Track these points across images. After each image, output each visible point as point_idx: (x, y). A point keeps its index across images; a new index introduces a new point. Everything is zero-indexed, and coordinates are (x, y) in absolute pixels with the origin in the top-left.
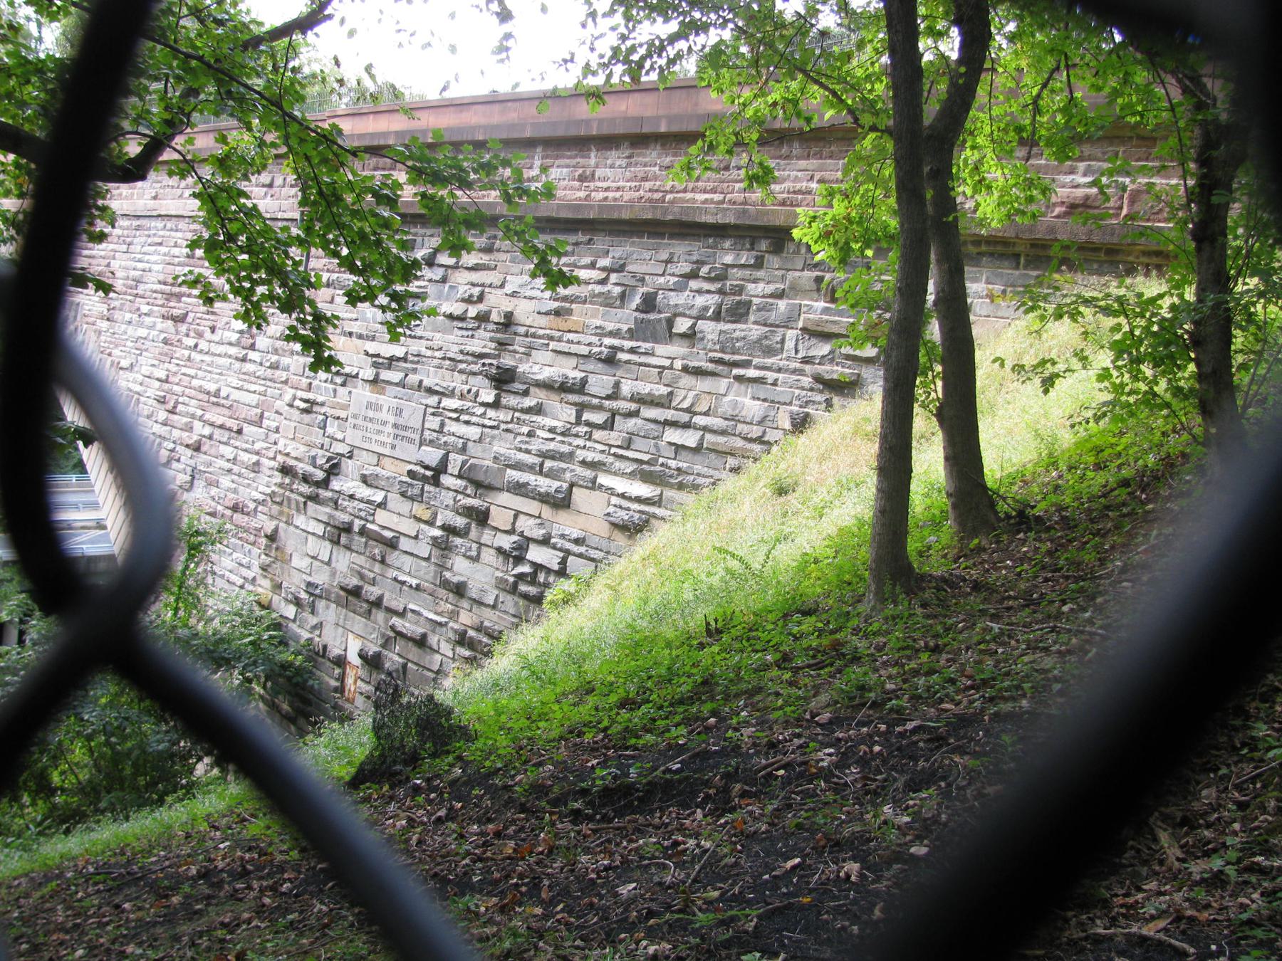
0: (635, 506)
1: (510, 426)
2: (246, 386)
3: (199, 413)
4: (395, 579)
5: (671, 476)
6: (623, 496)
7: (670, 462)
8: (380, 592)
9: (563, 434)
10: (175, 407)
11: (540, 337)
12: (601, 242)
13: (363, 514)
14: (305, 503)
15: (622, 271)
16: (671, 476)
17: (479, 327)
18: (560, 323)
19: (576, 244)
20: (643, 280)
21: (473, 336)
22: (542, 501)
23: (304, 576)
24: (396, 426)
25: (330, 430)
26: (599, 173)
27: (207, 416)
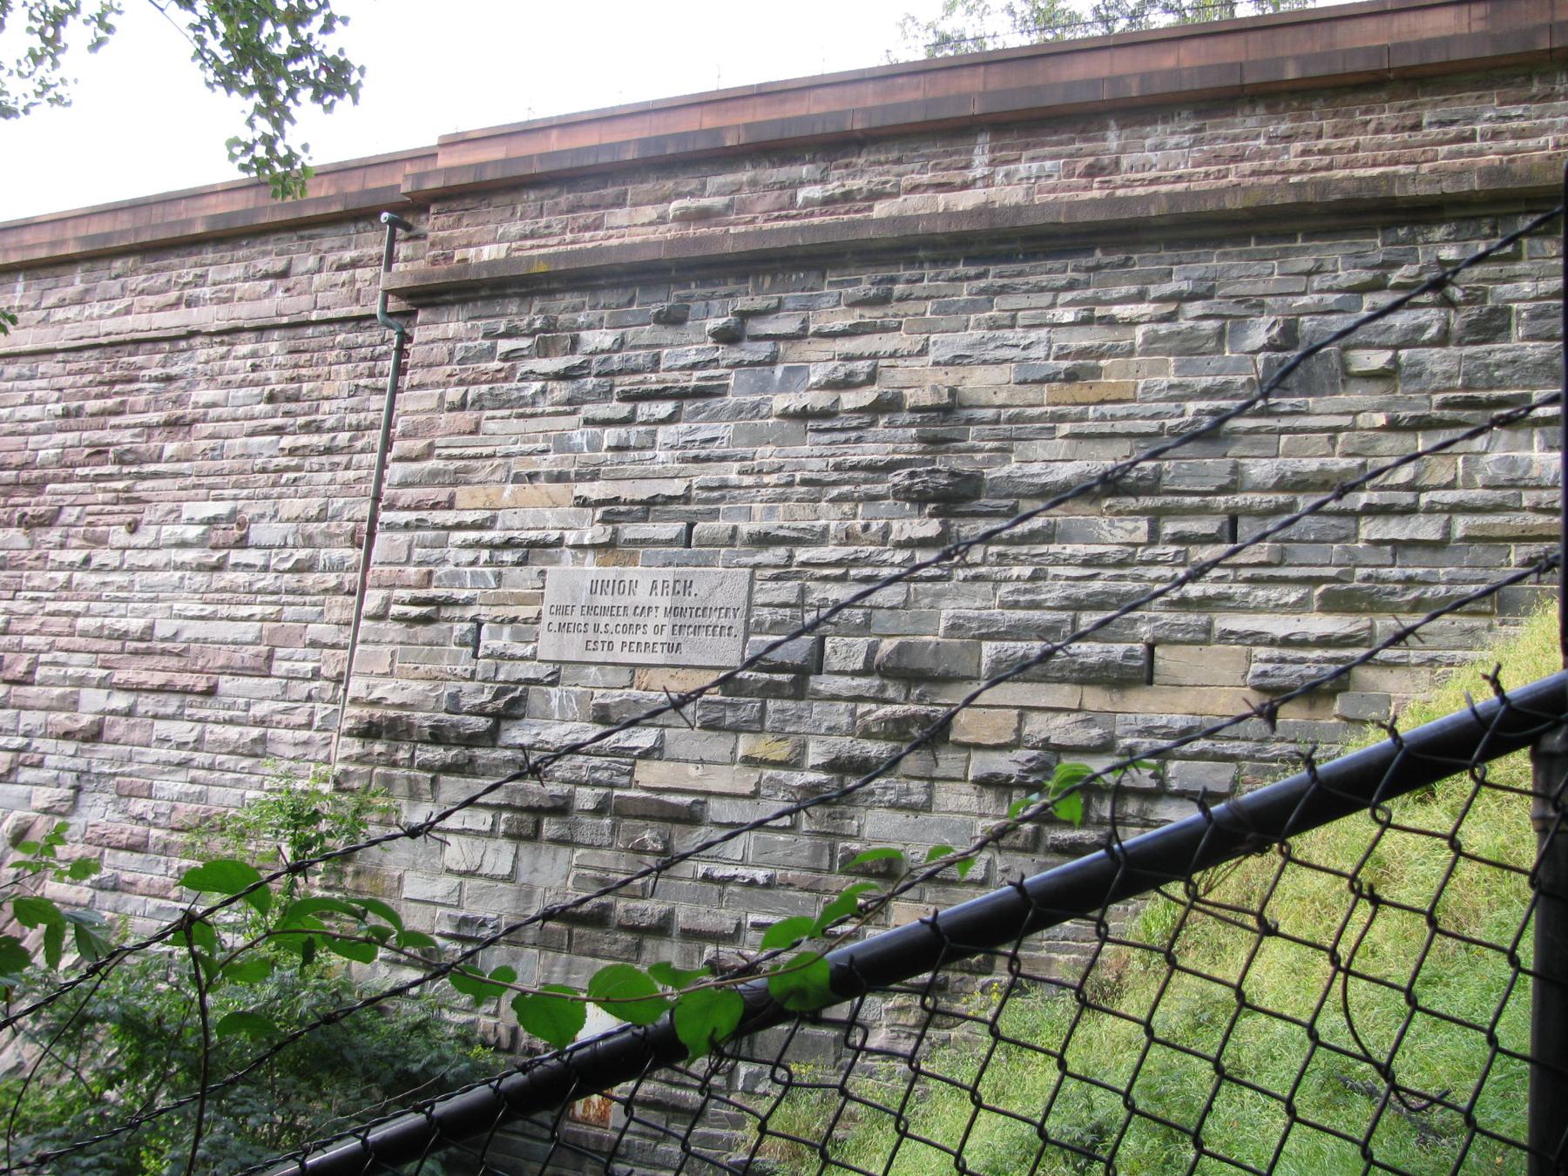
0: (1317, 653)
1: (983, 570)
2: (224, 610)
3: (99, 673)
4: (707, 878)
5: (1392, 593)
6: (1286, 642)
7: (1384, 572)
8: (665, 907)
9: (1121, 564)
10: (30, 672)
11: (1031, 420)
12: (1144, 262)
13: (603, 776)
14: (434, 781)
15: (1211, 297)
16: (1392, 593)
17: (873, 424)
18: (1077, 390)
19: (1097, 268)
20: (1261, 305)
21: (859, 440)
22: (1082, 682)
23: (453, 912)
24: (676, 611)
25: (488, 642)
26: (1125, 162)
27: (119, 676)
